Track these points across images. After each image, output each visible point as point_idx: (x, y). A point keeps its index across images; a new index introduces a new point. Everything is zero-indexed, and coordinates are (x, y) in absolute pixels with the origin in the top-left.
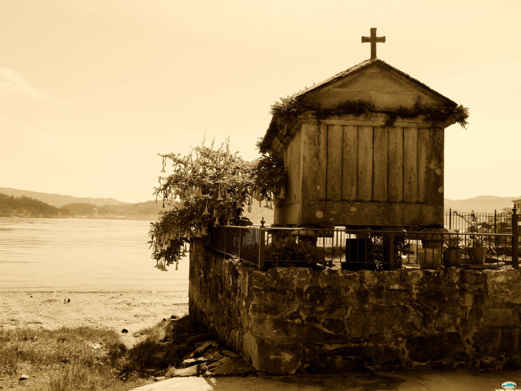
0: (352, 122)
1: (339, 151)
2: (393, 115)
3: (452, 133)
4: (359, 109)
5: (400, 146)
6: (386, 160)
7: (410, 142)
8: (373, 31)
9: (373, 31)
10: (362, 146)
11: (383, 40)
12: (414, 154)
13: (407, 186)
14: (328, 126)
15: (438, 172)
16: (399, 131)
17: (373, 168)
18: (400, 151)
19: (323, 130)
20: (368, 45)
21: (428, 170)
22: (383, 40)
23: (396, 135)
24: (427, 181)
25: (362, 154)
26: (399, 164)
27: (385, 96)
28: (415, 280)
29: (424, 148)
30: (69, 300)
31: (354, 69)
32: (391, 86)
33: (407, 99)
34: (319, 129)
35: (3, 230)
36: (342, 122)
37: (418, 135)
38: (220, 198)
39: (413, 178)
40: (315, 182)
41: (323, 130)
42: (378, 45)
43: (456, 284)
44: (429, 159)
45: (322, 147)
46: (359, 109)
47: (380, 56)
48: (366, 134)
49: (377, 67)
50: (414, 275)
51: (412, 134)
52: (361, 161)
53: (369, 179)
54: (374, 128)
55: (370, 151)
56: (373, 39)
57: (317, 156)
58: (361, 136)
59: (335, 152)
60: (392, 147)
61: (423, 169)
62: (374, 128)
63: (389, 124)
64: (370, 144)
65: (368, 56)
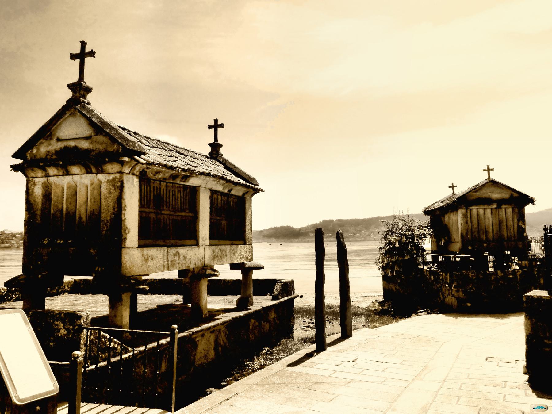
0: (482, 207)
1: (476, 220)
2: (500, 203)
3: (529, 209)
4: (487, 201)
5: (504, 216)
6: (498, 223)
7: (509, 214)
8: (488, 166)
9: (488, 166)
10: (487, 216)
11: (493, 170)
12: (511, 219)
13: (509, 234)
14: (471, 210)
15: (523, 226)
16: (504, 210)
17: (493, 226)
18: (505, 218)
19: (469, 211)
20: (487, 172)
21: (518, 226)
22: (493, 170)
23: (502, 212)
24: (518, 230)
25: (487, 221)
26: (505, 224)
27: (496, 195)
28: (518, 273)
29: (516, 216)
30: (302, 296)
31: (481, 184)
32: (499, 190)
33: (506, 195)
34: (467, 212)
35: (3, 255)
36: (477, 207)
37: (513, 210)
38: (416, 241)
39: (512, 230)
40: (467, 234)
41: (469, 211)
42: (491, 172)
43: (260, 324)
44: (518, 221)
45: (469, 219)
46: (487, 201)
47: (492, 177)
48: (489, 212)
49: (493, 183)
50: (518, 272)
51: (510, 210)
52: (487, 224)
53: (491, 231)
54: (491, 209)
55: (491, 219)
56: (488, 170)
57: (467, 223)
58: (486, 213)
59: (475, 221)
60: (500, 216)
61: (516, 226)
62: (491, 209)
63: (499, 207)
64: (490, 216)
65: (487, 178)
